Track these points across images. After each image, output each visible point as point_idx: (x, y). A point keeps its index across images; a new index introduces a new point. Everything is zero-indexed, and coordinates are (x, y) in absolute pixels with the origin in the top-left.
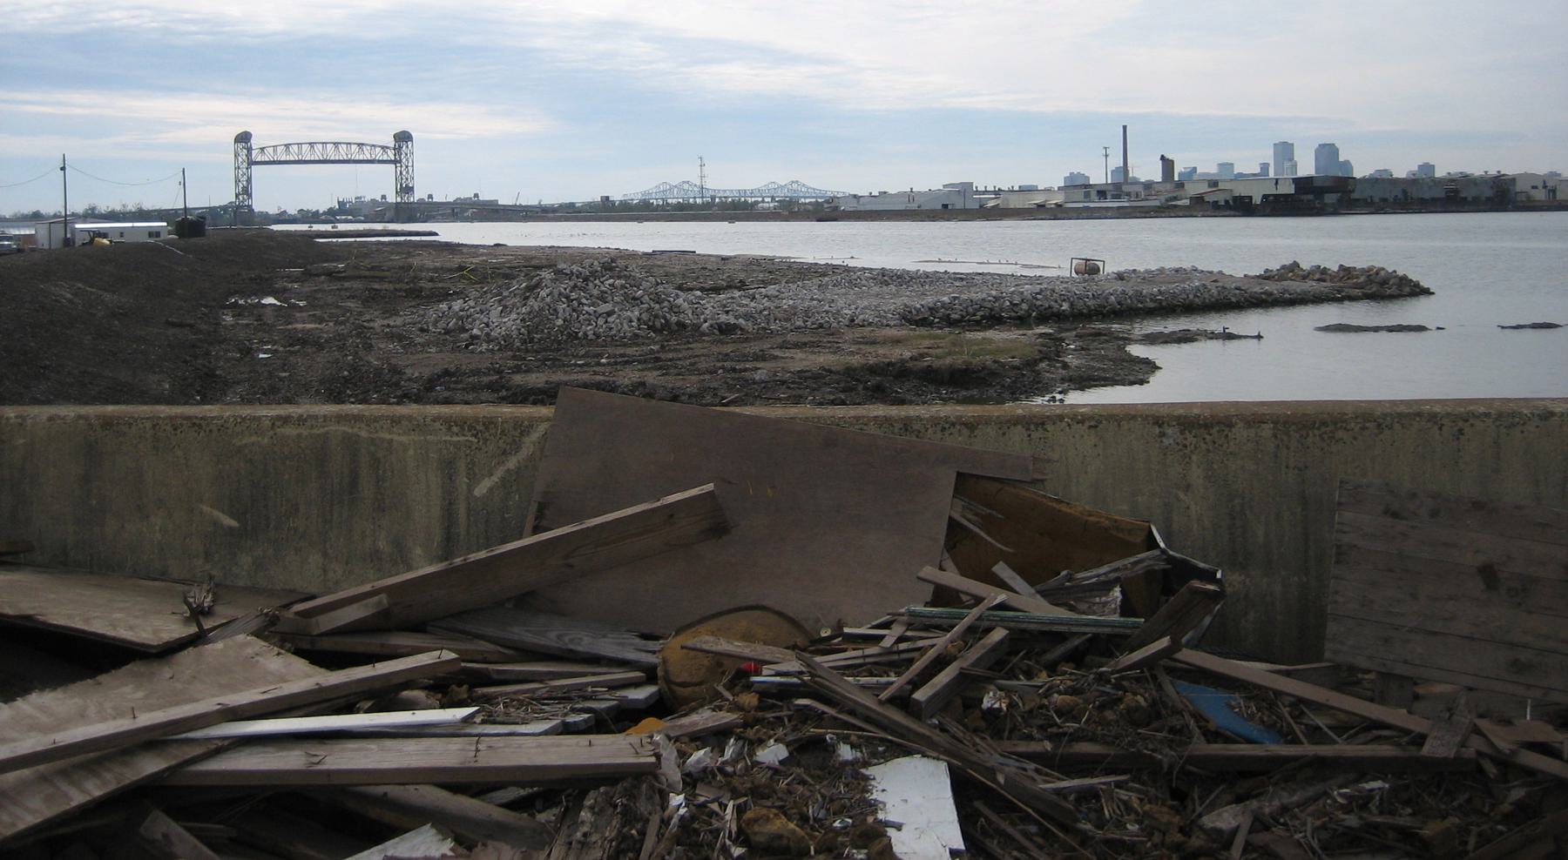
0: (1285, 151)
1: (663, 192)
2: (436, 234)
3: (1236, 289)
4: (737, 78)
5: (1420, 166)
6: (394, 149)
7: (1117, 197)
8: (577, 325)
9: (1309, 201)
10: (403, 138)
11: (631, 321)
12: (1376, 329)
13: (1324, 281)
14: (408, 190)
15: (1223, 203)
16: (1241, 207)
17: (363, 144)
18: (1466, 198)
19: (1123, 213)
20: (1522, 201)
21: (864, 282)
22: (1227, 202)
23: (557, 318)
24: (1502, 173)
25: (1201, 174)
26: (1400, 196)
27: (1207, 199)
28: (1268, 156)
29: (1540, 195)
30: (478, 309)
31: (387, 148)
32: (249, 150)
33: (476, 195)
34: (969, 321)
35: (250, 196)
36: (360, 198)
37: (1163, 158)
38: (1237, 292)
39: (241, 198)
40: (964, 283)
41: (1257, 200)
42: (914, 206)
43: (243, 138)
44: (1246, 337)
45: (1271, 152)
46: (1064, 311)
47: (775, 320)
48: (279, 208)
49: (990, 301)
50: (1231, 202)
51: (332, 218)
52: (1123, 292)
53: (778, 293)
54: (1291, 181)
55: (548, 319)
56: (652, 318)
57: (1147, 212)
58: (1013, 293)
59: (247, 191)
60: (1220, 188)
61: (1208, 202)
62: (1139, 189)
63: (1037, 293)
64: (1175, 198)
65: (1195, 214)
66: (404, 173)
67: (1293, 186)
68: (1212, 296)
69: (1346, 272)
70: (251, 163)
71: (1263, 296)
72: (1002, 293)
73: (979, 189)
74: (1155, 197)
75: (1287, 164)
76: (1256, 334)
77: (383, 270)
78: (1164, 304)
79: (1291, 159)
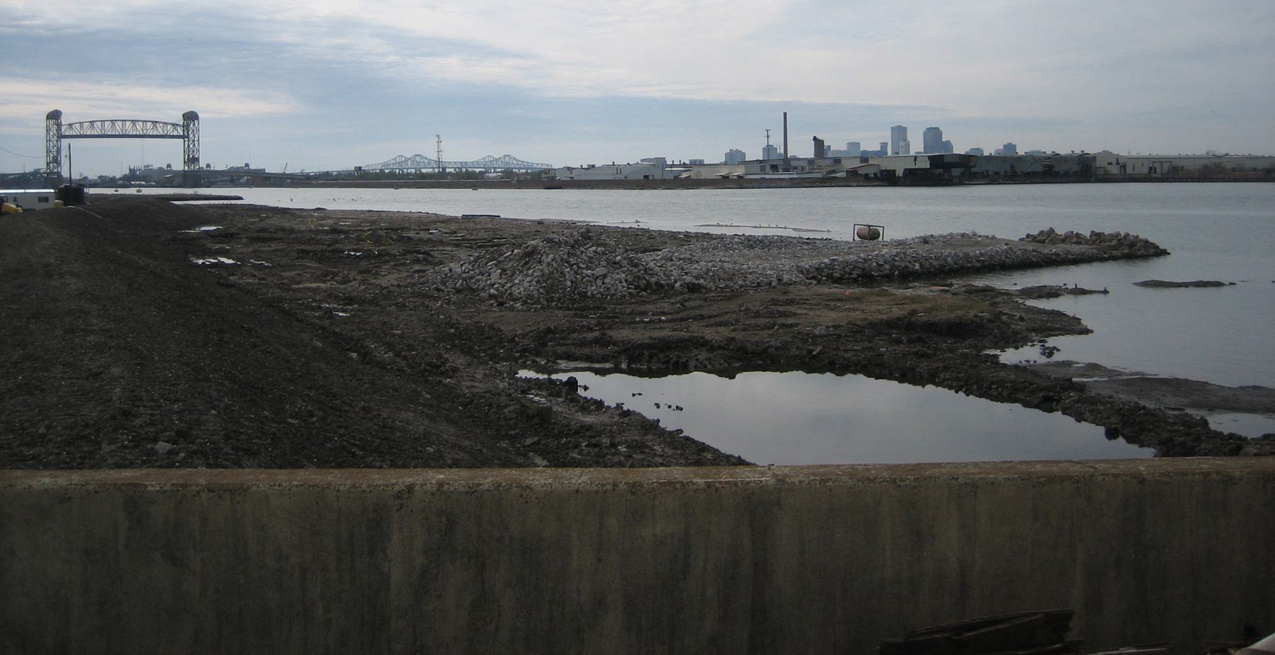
0: (900, 133)
1: (399, 163)
2: (242, 199)
3: (1033, 251)
4: (451, 69)
5: (1004, 146)
6: (183, 127)
7: (786, 170)
8: (583, 286)
9: (939, 174)
10: (191, 117)
11: (621, 282)
12: (1186, 285)
13: (1080, 243)
14: (195, 160)
15: (872, 176)
16: (887, 178)
17: (157, 122)
18: (1059, 172)
19: (794, 184)
20: (1101, 175)
21: (735, 246)
22: (875, 174)
23: (566, 280)
24: (1085, 152)
25: (834, 152)
26: (1009, 169)
27: (860, 172)
28: (887, 137)
29: (1114, 170)
30: (477, 271)
31: (177, 125)
32: (59, 126)
33: (247, 165)
34: (848, 278)
35: (59, 164)
36: (149, 166)
37: (815, 138)
38: (1035, 253)
39: (51, 165)
40: (810, 246)
41: (900, 173)
42: (621, 177)
43: (54, 116)
44: (1091, 292)
45: (889, 133)
46: (917, 270)
47: (720, 280)
48: (81, 174)
49: (860, 262)
50: (879, 175)
51: (128, 183)
52: (955, 255)
53: (690, 257)
54: (927, 158)
55: (559, 281)
56: (636, 280)
57: (813, 183)
58: (877, 255)
59: (56, 160)
60: (870, 163)
61: (861, 175)
62: (804, 164)
63: (894, 256)
64: (834, 172)
65: (852, 184)
66: (191, 146)
67: (929, 162)
68: (1017, 257)
69: (1097, 237)
70: (61, 137)
71: (1054, 257)
72: (868, 256)
73: (675, 163)
74: (817, 171)
75: (902, 144)
76: (1103, 289)
77: (271, 232)
78: (986, 263)
79: (905, 140)
